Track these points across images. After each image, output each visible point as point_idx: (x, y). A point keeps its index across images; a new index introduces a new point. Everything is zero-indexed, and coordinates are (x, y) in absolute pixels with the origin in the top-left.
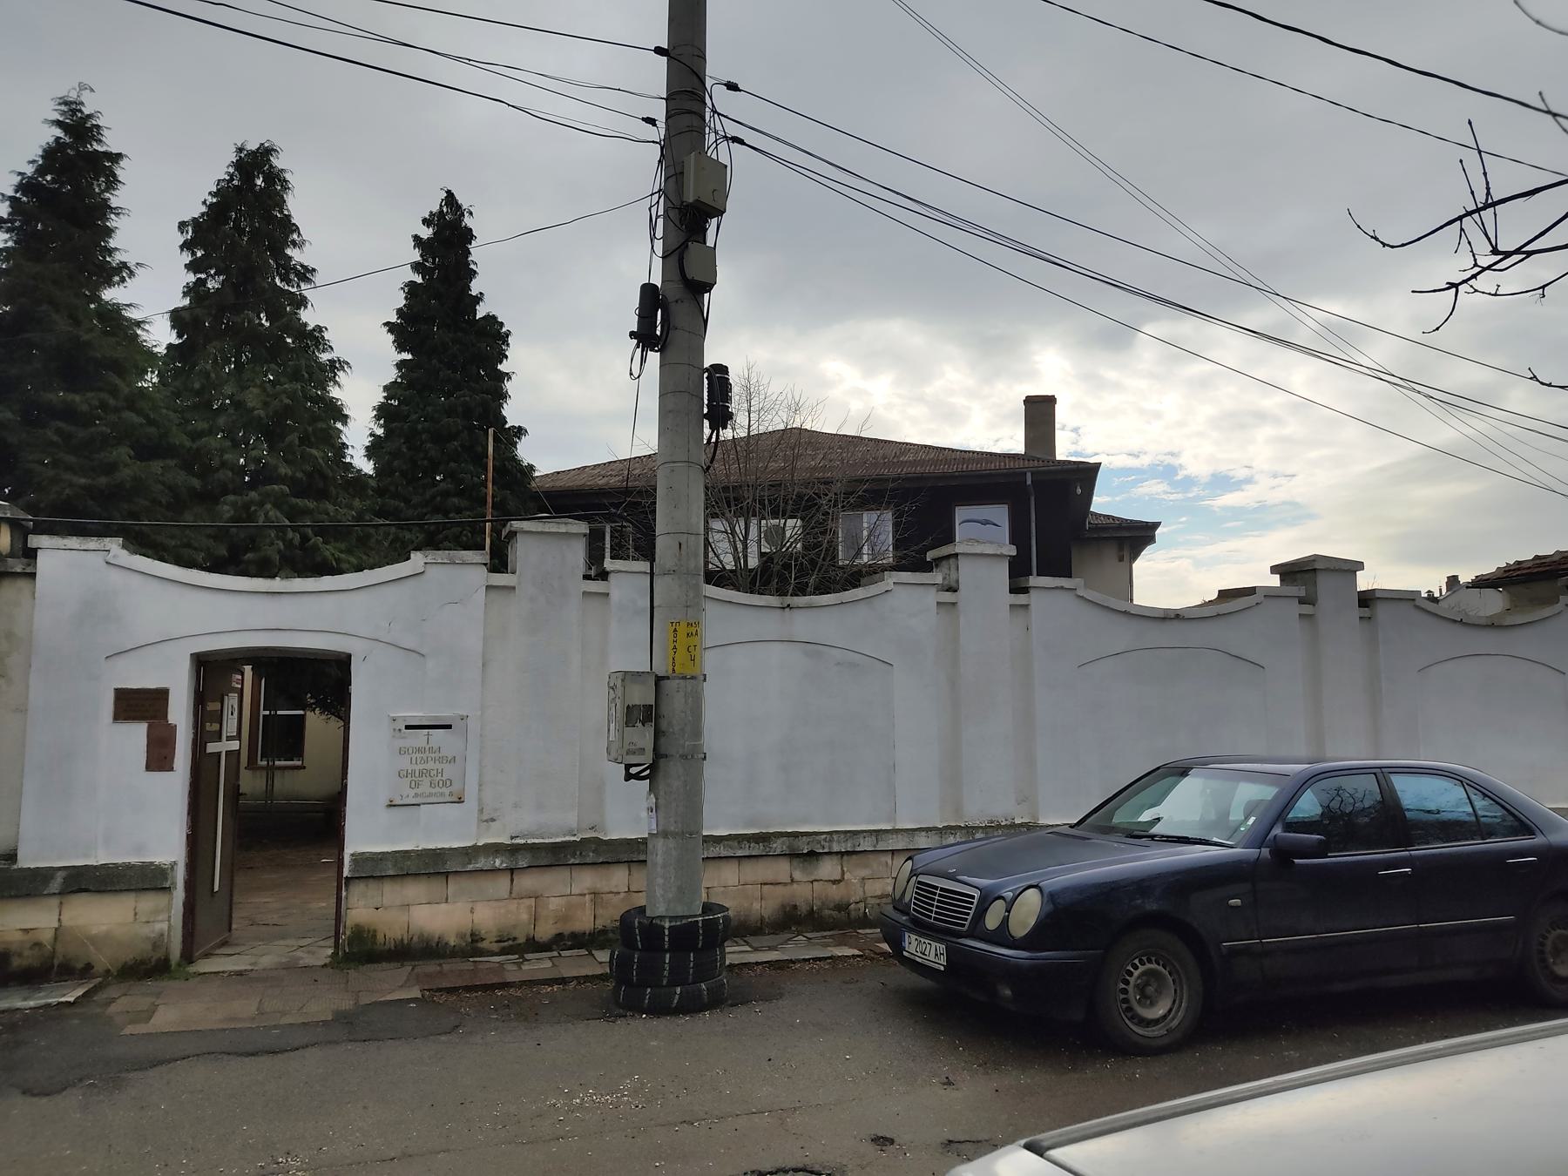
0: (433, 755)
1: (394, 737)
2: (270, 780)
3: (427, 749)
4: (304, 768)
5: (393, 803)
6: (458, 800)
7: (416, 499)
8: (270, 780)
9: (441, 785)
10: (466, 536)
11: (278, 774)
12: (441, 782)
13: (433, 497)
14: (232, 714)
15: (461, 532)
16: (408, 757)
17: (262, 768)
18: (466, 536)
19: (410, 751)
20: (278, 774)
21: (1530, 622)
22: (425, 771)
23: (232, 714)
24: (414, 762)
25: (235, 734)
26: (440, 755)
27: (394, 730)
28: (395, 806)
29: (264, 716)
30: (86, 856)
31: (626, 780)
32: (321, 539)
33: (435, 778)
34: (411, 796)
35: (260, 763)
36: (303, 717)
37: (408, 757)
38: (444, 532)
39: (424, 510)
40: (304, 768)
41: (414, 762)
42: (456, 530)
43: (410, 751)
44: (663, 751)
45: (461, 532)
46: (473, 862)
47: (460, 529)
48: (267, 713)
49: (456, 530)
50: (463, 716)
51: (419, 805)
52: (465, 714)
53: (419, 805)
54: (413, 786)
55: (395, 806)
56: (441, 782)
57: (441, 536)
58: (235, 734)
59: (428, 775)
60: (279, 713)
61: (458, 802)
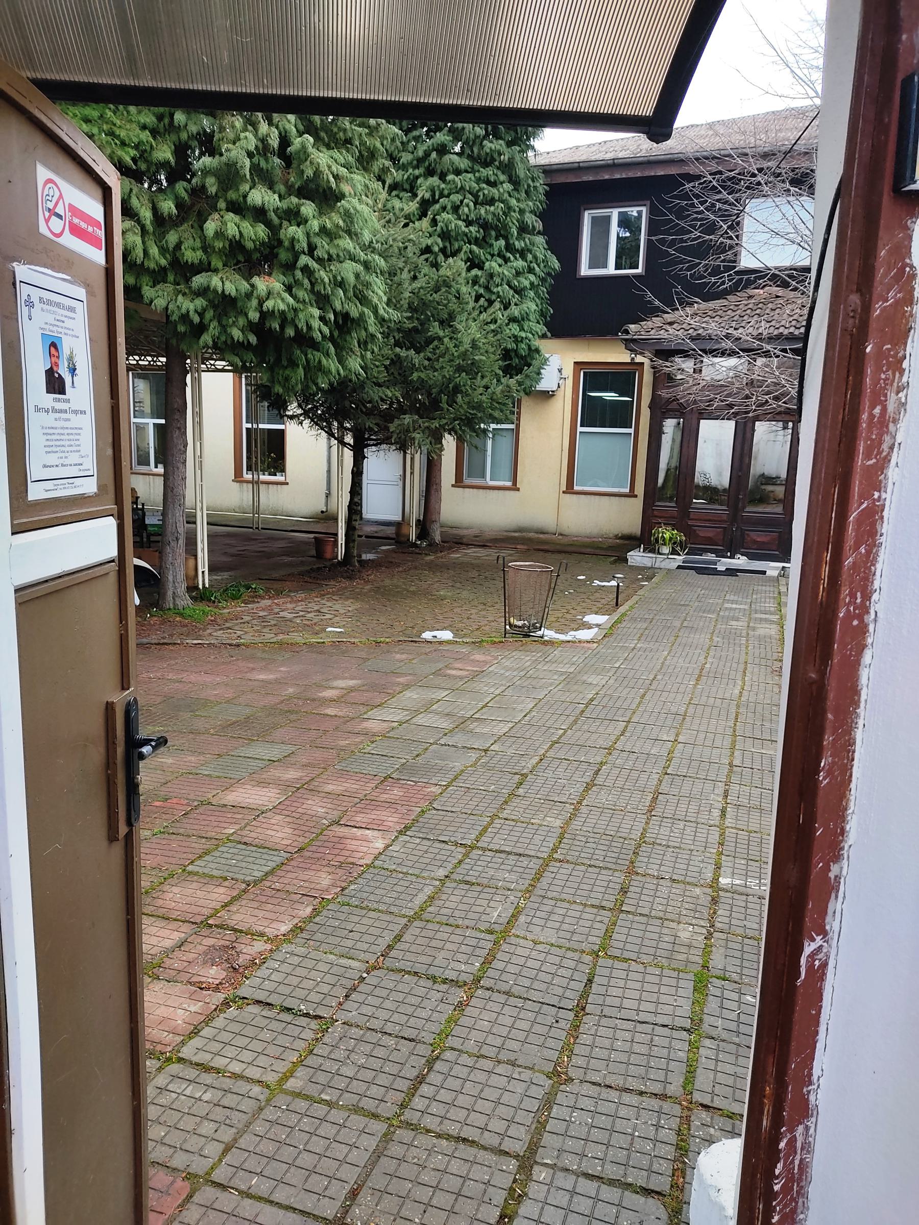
2: (256, 495)
4: (287, 484)
7: (406, 158)
8: (256, 495)
10: (468, 206)
11: (263, 487)
13: (427, 154)
14: (55, 384)
15: (462, 202)
17: (247, 482)
18: (468, 206)
20: (263, 487)
23: (55, 384)
25: (90, 487)
29: (247, 429)
31: (518, 490)
32: (311, 139)
35: (245, 475)
36: (282, 433)
38: (441, 200)
39: (417, 172)
40: (287, 484)
42: (456, 198)
45: (462, 202)
47: (461, 198)
48: (249, 426)
49: (456, 198)
57: (437, 206)
58: (90, 487)
60: (261, 426)
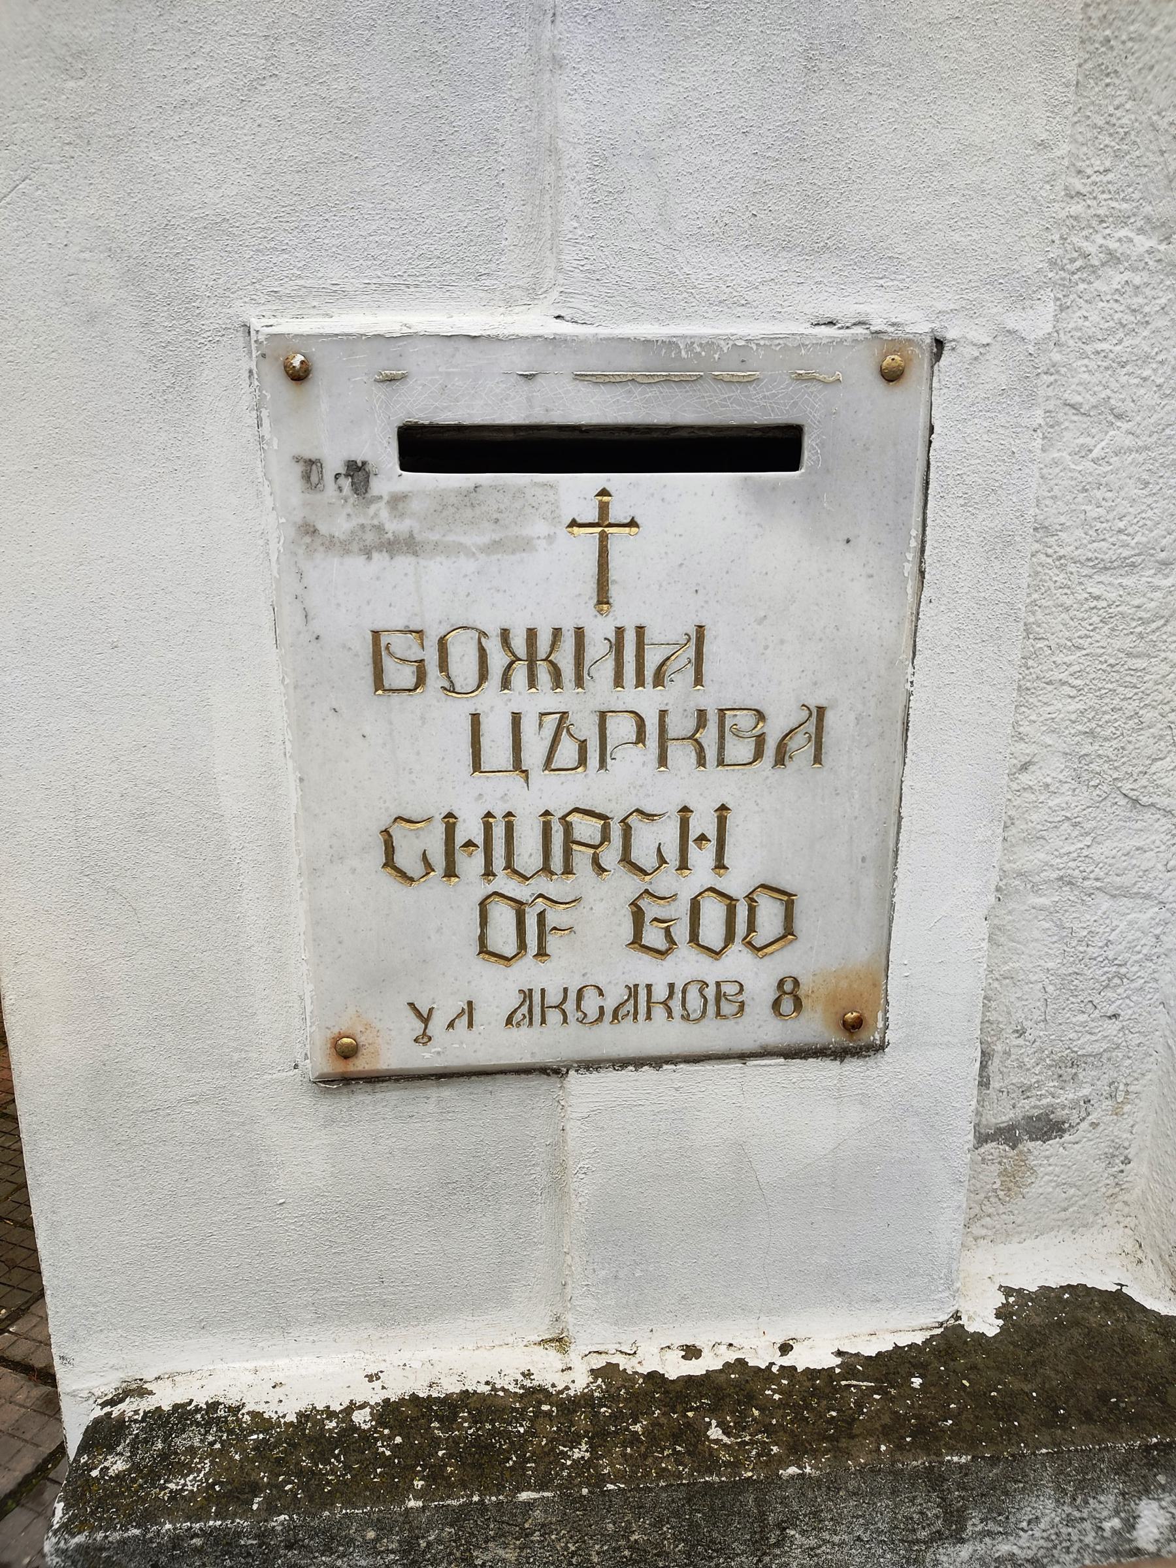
0: (648, 701)
1: (309, 530)
3: (596, 648)
5: (361, 1065)
6: (835, 1037)
9: (712, 930)
12: (713, 914)
16: (458, 711)
19: (464, 665)
21: (927, 488)
22: (587, 829)
24: (497, 751)
26: (710, 698)
27: (310, 468)
28: (375, 1079)
30: (746, 479)
33: (665, 882)
34: (492, 1011)
37: (458, 711)
41: (497, 751)
43: (464, 665)
44: (628, 520)
46: (974, 1524)
50: (899, 345)
51: (553, 1071)
52: (920, 326)
53: (553, 1071)
54: (503, 935)
55: (375, 1079)
56: (713, 914)
59: (610, 856)
61: (840, 1054)
